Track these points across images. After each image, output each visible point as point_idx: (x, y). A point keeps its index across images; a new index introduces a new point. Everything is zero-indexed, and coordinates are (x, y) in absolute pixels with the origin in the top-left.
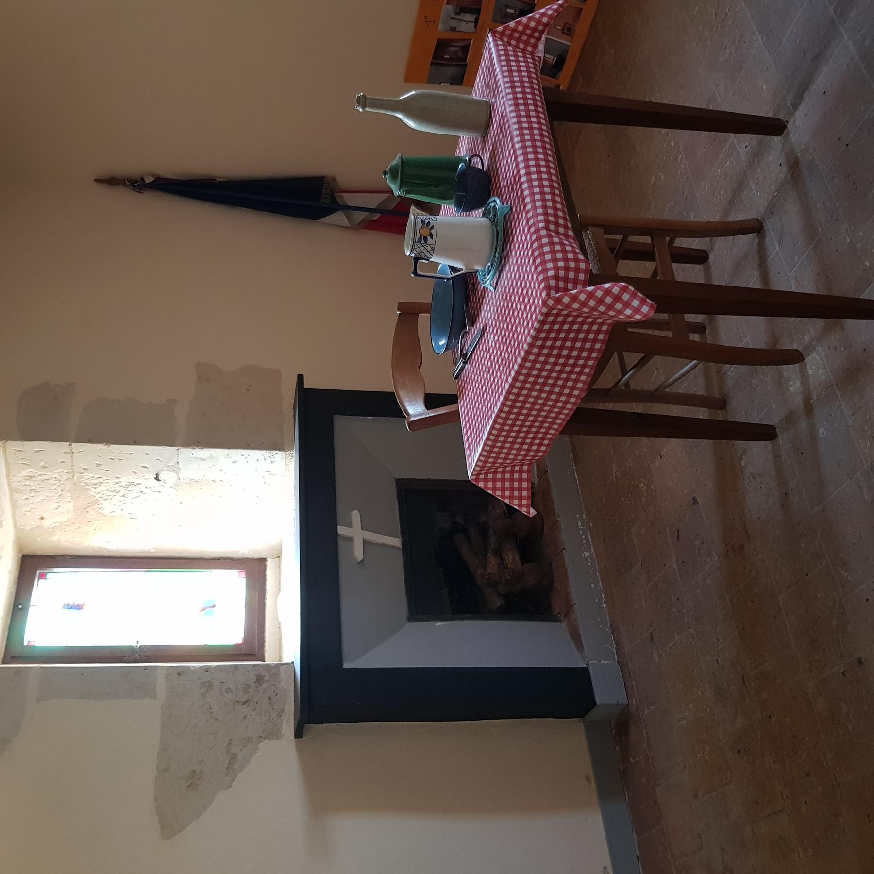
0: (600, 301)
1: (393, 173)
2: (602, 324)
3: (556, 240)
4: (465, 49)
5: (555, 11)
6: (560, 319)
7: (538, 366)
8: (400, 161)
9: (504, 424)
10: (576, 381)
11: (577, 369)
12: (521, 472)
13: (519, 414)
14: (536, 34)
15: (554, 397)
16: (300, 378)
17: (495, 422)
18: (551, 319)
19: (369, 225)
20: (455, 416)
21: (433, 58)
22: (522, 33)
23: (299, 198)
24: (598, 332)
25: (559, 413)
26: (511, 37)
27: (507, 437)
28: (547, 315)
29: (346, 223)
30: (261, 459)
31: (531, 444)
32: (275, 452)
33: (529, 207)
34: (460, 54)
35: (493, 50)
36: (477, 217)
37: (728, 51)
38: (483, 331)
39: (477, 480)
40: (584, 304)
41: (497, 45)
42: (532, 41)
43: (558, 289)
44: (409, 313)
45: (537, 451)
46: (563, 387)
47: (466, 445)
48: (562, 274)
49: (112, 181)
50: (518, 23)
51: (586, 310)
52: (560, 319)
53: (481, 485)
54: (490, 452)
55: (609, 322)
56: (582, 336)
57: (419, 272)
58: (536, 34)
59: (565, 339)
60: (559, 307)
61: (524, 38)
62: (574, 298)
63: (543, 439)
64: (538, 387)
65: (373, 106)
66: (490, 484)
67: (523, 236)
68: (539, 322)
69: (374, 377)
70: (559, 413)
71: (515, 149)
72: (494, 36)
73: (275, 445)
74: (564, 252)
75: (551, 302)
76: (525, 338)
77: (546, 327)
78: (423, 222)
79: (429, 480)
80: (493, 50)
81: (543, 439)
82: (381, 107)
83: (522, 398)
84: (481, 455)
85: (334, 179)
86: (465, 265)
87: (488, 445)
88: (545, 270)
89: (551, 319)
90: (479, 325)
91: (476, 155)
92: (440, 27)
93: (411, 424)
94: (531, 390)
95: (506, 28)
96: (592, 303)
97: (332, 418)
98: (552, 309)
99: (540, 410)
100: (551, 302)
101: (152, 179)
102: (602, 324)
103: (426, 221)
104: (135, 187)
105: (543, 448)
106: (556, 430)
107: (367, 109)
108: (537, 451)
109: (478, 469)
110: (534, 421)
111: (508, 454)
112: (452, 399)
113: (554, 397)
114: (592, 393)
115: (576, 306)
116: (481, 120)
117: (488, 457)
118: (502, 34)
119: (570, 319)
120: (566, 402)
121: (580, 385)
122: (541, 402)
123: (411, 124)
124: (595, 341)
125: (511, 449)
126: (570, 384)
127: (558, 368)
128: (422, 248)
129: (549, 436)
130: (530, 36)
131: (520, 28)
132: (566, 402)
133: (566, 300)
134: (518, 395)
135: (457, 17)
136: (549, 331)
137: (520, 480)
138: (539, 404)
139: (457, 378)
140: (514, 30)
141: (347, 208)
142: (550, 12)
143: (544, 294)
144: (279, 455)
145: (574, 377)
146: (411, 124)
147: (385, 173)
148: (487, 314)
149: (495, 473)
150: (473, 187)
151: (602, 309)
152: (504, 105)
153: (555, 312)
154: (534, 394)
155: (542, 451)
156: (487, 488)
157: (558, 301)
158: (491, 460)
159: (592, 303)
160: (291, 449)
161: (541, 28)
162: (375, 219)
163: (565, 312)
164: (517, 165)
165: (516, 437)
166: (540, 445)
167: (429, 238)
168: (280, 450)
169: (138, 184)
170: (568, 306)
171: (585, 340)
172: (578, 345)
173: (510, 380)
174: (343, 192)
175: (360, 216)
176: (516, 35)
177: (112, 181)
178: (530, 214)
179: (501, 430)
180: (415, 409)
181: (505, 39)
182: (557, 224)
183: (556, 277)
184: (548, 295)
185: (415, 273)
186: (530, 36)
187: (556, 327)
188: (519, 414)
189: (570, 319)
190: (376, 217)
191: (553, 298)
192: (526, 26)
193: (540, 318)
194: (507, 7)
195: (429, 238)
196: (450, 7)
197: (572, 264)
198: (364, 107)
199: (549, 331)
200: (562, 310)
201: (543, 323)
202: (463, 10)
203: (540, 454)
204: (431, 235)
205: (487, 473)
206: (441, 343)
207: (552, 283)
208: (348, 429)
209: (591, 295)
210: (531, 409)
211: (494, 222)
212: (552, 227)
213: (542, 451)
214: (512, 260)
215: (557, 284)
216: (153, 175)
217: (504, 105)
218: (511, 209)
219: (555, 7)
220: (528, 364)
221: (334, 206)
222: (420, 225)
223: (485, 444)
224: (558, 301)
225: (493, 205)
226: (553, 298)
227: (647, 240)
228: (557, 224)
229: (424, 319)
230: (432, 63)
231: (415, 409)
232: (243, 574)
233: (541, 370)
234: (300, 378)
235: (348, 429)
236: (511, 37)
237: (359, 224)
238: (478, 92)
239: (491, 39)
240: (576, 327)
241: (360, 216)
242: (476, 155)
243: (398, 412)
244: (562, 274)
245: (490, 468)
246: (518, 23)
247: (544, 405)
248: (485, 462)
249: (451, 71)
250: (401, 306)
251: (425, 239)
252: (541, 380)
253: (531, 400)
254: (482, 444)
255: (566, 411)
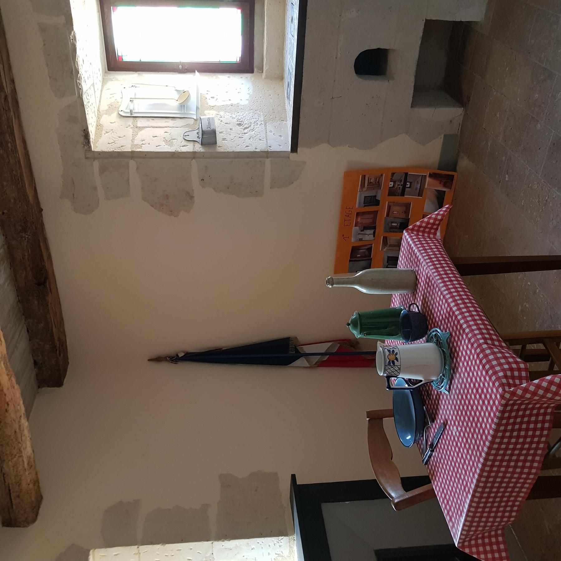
0: (547, 390)
1: (354, 323)
2: (547, 408)
3: (496, 350)
4: (370, 250)
5: (445, 211)
6: (516, 407)
7: (503, 446)
8: (358, 315)
9: (481, 498)
10: (534, 455)
11: (534, 446)
12: (496, 536)
13: (492, 487)
14: (435, 227)
15: (511, 470)
16: (293, 477)
17: (473, 496)
18: (509, 408)
19: (322, 364)
20: (431, 494)
21: (351, 258)
22: (425, 227)
23: (275, 353)
24: (545, 414)
25: (524, 483)
26: (418, 231)
27: (485, 507)
28: (505, 406)
29: (307, 365)
30: (272, 544)
31: (490, 512)
32: (281, 538)
33: (467, 330)
34: (367, 253)
35: (409, 240)
36: (421, 344)
37: (554, 221)
38: (445, 424)
39: (463, 547)
40: (534, 394)
41: (411, 237)
42: (433, 231)
43: (510, 386)
44: (375, 419)
45: (510, 517)
46: (517, 461)
47: (448, 519)
48: (509, 373)
49: (158, 359)
50: (422, 222)
51: (536, 398)
52: (516, 407)
53: (467, 551)
54: (472, 522)
55: (553, 405)
56: (533, 419)
57: (392, 387)
58: (435, 227)
59: (521, 423)
60: (515, 398)
61: (427, 230)
62: (526, 390)
63: (513, 506)
64: (505, 464)
65: (338, 283)
66: (474, 550)
67: (467, 351)
68: (500, 412)
69: (360, 469)
70: (524, 483)
71: (444, 295)
72: (407, 232)
73: (281, 532)
74: (505, 358)
75: (507, 396)
76: (488, 424)
77: (506, 415)
78: (389, 351)
79: (400, 549)
80: (409, 240)
81: (513, 506)
82: (343, 283)
83: (493, 474)
84: (464, 525)
85: (296, 338)
86: (424, 378)
87: (470, 516)
88: (495, 373)
89: (509, 408)
90: (440, 420)
91: (412, 304)
92: (353, 240)
93: (396, 505)
94: (500, 466)
95: (415, 226)
96: (541, 392)
97: (320, 508)
98: (509, 400)
99: (508, 483)
100: (507, 396)
101: (183, 354)
102: (547, 408)
103: (391, 350)
104: (172, 361)
105: (514, 514)
106: (523, 497)
107: (334, 286)
108: (510, 517)
109: (463, 537)
110: (505, 492)
111: (487, 522)
112: (426, 480)
113: (511, 470)
114: (549, 461)
115: (528, 396)
116: (411, 283)
117: (470, 526)
118: (412, 230)
119: (523, 407)
120: (529, 474)
121: (537, 458)
122: (508, 475)
123: (364, 290)
124: (544, 422)
125: (488, 517)
126: (522, 458)
127: (511, 446)
128: (392, 369)
129: (517, 503)
130: (431, 228)
131: (424, 225)
132: (529, 474)
133: (519, 392)
134: (490, 472)
135: (362, 233)
136: (509, 418)
137: (498, 543)
138: (515, 478)
139: (426, 463)
140: (420, 226)
141: (307, 355)
142: (441, 213)
143: (500, 390)
144: (284, 540)
145: (532, 452)
146: (364, 290)
147: (349, 325)
148: (445, 411)
149: (476, 539)
150: (414, 325)
151: (549, 395)
152: (426, 270)
153: (511, 402)
154: (503, 469)
155: (513, 517)
156: (472, 553)
157: (513, 394)
158: (473, 529)
159: (541, 392)
160: (293, 533)
161: (437, 222)
162: (325, 359)
163: (519, 402)
164: (449, 305)
165: (492, 507)
166: (511, 511)
167: (395, 361)
168: (285, 536)
169: (174, 359)
170: (522, 397)
171: (514, 424)
172: (532, 426)
173: (482, 460)
174: (302, 345)
175: (316, 359)
176: (422, 229)
177: (158, 359)
178: (470, 335)
179: (479, 503)
180: (395, 494)
181: (415, 233)
182: (492, 339)
183: (506, 376)
184: (504, 390)
185: (389, 387)
186: (431, 228)
187: (513, 414)
188: (499, 487)
189: (523, 407)
190: (326, 358)
191: (508, 392)
192: (428, 223)
193: (500, 408)
194: (392, 222)
195: (395, 361)
196: (357, 228)
197: (514, 366)
198: (332, 285)
199: (509, 418)
200: (517, 400)
201: (503, 412)
202: (365, 228)
203: (512, 519)
204: (397, 359)
205: (470, 540)
206: (408, 438)
207: (504, 381)
208: (334, 514)
209: (538, 386)
210: (501, 483)
211: (439, 344)
212: (489, 342)
213: (513, 517)
214: (461, 369)
215: (509, 381)
216: (183, 352)
217: (426, 270)
218: (451, 334)
219: (444, 209)
220: (496, 446)
221: (298, 355)
222: (387, 353)
223: (467, 516)
224: (513, 394)
225: (434, 333)
226: (508, 392)
227: (541, 346)
228: (492, 339)
229: (388, 423)
230: (350, 261)
231: (395, 494)
232: (239, 11)
233: (506, 449)
234: (293, 477)
235: (334, 514)
236: (418, 231)
237: (315, 364)
238: (402, 265)
239: (406, 234)
240: (521, 413)
241: (316, 359)
242: (412, 304)
243: (381, 495)
244: (509, 373)
245: (473, 535)
246: (422, 222)
247: (511, 478)
248: (469, 531)
249: (363, 263)
250: (369, 414)
251: (393, 362)
252: (507, 458)
253: (501, 475)
254: (464, 515)
255: (529, 481)
